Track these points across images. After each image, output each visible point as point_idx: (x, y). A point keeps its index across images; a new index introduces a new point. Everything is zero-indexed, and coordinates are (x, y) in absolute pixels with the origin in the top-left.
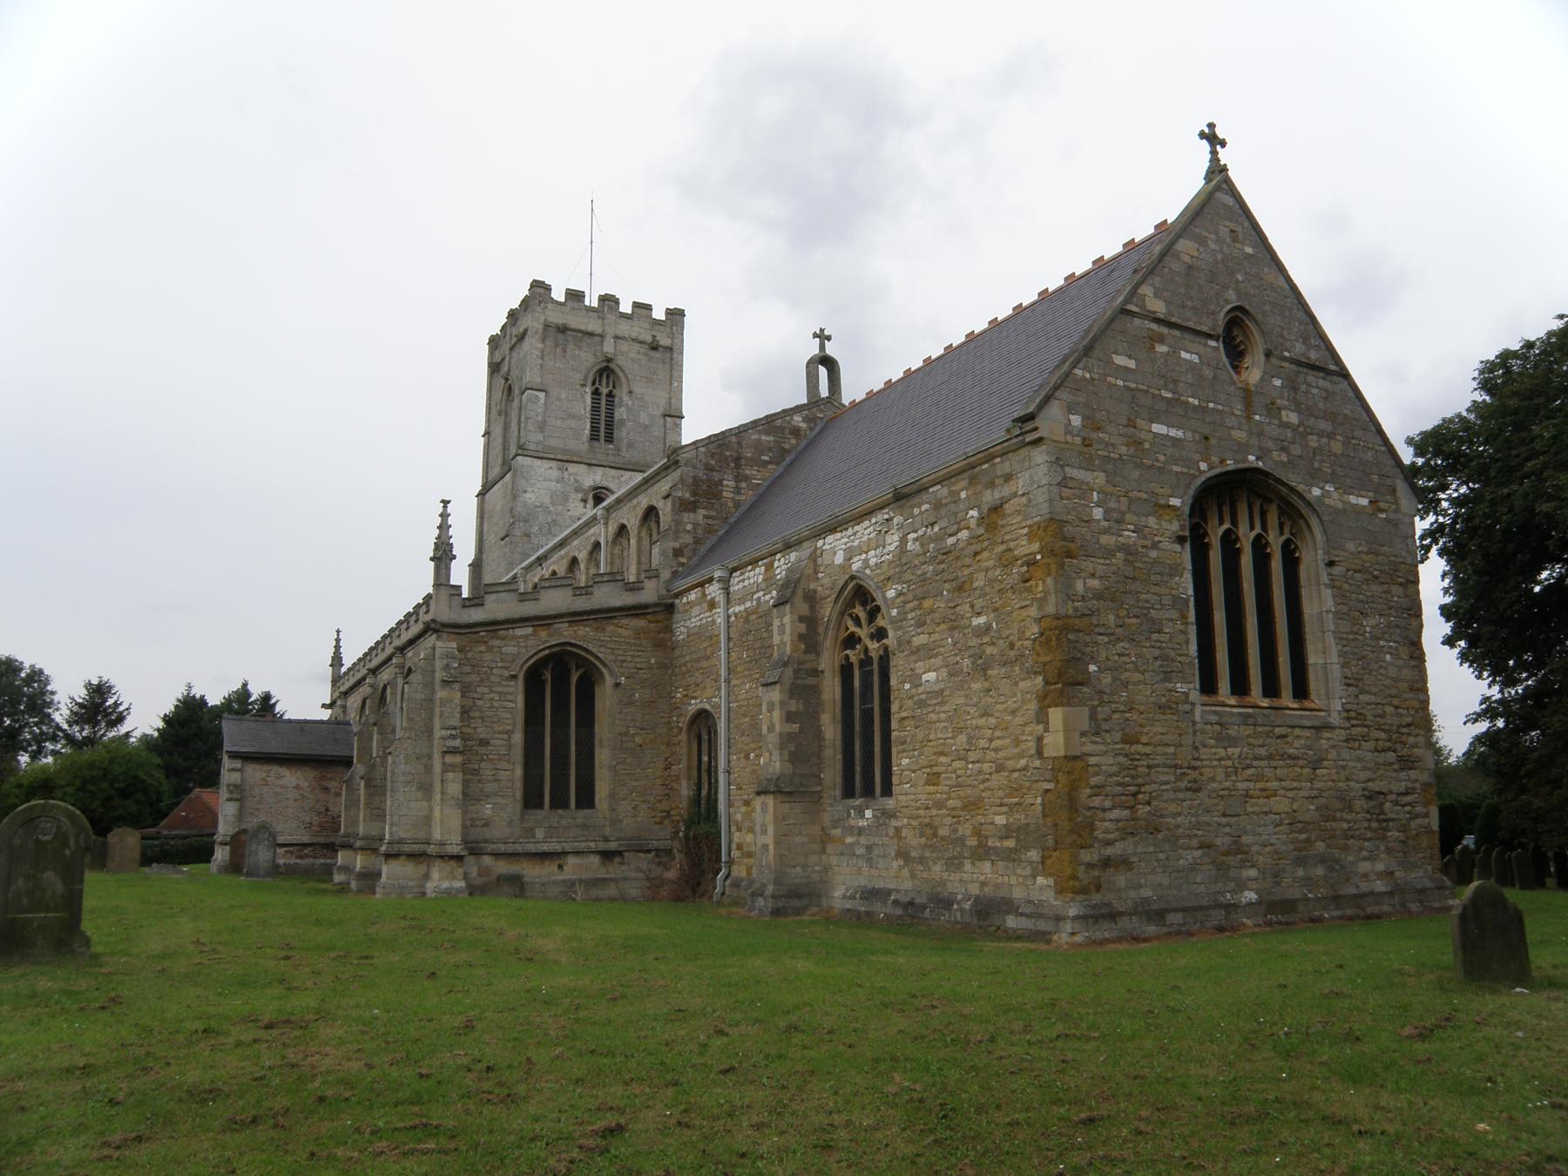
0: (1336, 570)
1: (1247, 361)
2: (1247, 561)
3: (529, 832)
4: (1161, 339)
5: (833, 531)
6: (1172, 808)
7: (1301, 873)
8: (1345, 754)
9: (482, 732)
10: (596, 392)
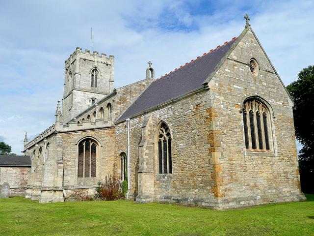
0: (275, 119)
1: (255, 70)
2: (255, 117)
3: (79, 183)
4: (236, 65)
5: (157, 110)
6: (240, 176)
7: (270, 191)
8: (279, 163)
9: (68, 159)
10: (93, 75)
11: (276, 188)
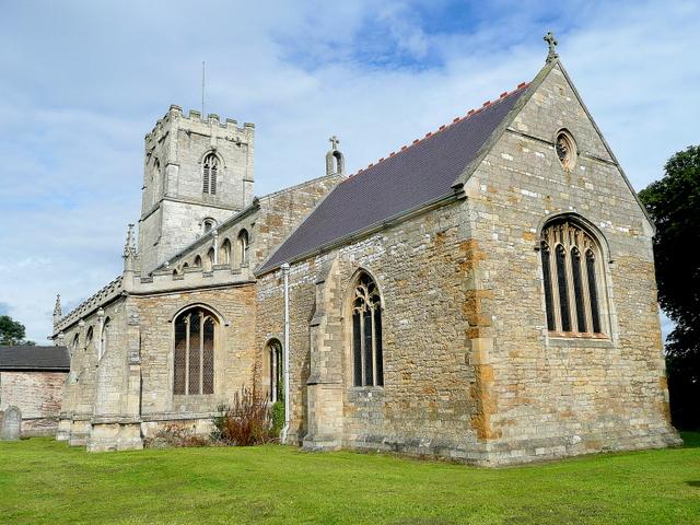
0: (613, 266)
1: (568, 156)
2: (568, 261)
3: (177, 408)
4: (525, 145)
5: (349, 244)
6: (535, 391)
7: (602, 425)
8: (621, 362)
9: (151, 353)
10: (206, 167)
11: (616, 419)
